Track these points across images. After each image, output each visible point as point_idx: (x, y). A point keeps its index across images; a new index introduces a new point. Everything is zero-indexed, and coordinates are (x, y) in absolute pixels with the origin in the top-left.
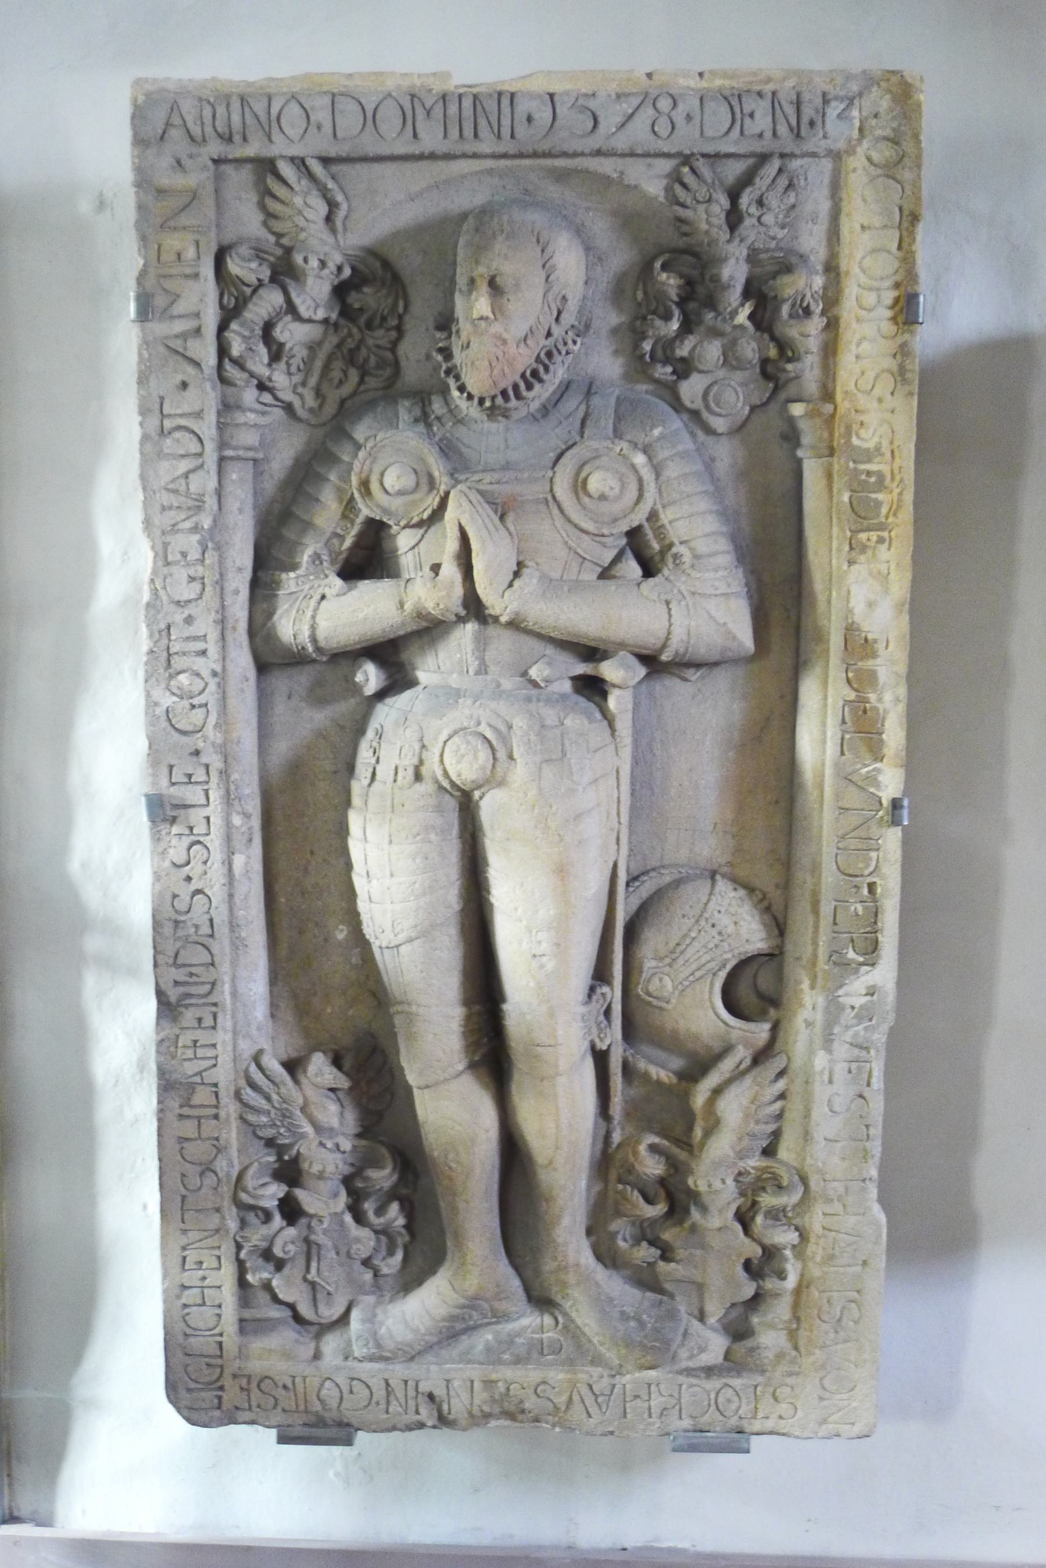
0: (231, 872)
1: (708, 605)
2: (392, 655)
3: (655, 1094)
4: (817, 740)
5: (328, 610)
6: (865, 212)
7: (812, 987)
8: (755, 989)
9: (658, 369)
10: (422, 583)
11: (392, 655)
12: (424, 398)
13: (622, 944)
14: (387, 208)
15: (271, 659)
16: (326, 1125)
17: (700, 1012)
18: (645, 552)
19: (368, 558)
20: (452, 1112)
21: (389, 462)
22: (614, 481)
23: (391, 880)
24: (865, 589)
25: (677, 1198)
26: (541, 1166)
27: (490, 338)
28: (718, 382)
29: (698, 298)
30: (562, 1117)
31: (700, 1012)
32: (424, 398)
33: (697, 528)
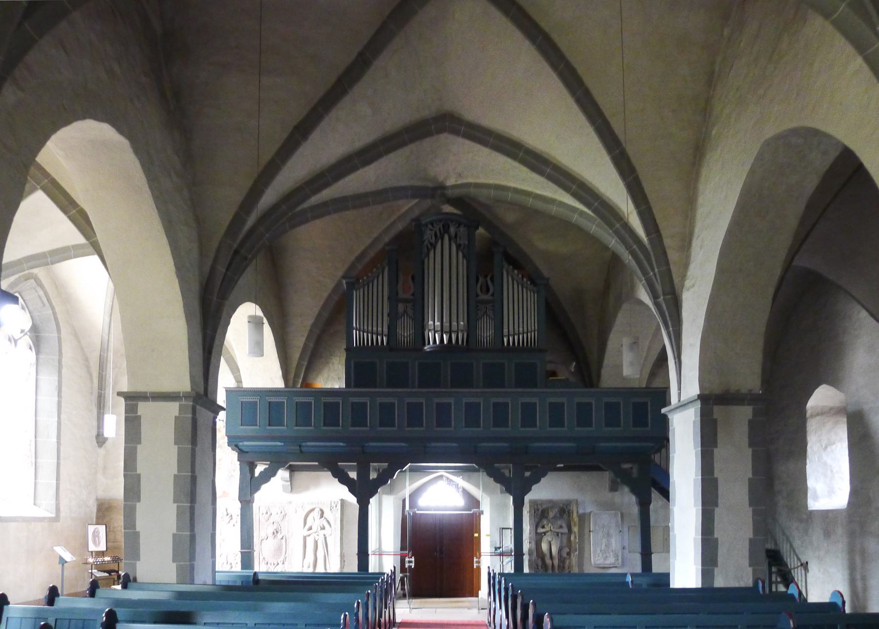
0: (534, 546)
1: (565, 530)
2: (545, 533)
3: (562, 560)
4: (572, 538)
5: (541, 530)
6: (575, 508)
7: (104, 350)
8: (569, 554)
9: (561, 516)
10: (547, 528)
11: (545, 533)
12: (547, 517)
13: (560, 551)
14: (544, 506)
15: (537, 533)
16: (540, 563)
17: (565, 555)
18: (561, 527)
19: (543, 527)
20: (548, 561)
21: (545, 522)
22: (559, 522)
23: (544, 547)
24: (575, 529)
25: (564, 568)
26: (810, 517)
27: (551, 515)
28: (565, 516)
29: (564, 512)
30: (556, 562)
31: (565, 555)
32: (547, 517)
33: (564, 525)
